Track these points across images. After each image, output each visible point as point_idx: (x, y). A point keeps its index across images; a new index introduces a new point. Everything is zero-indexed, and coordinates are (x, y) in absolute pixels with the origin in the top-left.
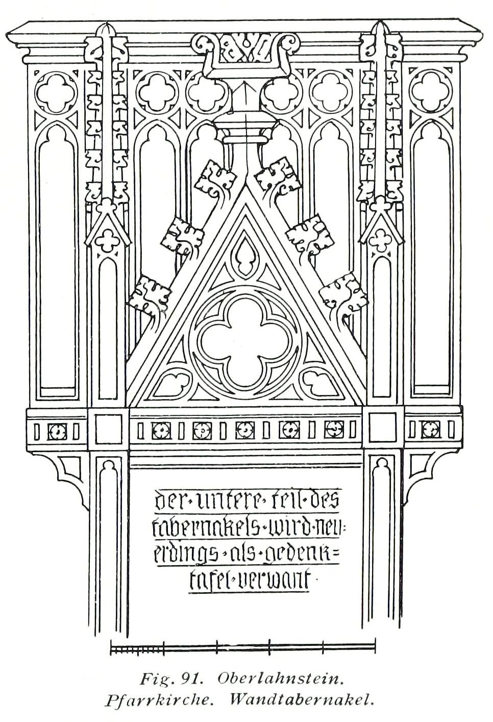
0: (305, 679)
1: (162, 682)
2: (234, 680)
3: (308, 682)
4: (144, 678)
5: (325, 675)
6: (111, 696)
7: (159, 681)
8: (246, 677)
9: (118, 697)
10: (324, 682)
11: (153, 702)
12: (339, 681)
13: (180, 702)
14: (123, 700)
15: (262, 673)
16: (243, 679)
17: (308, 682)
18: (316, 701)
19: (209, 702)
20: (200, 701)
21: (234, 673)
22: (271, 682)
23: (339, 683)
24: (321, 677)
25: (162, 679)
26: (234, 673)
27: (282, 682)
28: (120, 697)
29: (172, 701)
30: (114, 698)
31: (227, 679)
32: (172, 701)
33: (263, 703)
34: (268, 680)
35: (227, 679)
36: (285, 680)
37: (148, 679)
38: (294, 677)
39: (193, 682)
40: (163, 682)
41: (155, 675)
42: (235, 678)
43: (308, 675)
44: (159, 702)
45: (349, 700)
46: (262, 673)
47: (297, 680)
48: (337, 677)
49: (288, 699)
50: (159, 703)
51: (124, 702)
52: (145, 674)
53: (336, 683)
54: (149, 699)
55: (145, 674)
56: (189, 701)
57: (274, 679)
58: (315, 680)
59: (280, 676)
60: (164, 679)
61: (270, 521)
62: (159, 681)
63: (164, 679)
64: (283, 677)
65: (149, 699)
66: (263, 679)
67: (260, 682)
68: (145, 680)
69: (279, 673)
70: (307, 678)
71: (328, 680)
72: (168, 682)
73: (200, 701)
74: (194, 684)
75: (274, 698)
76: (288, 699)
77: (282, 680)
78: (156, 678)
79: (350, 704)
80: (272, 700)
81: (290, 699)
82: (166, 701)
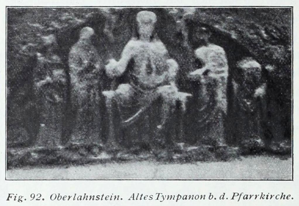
0: (100, 198)
1: (19, 199)
2: (59, 198)
3: (102, 199)
4: (9, 197)
5: (112, 195)
6: (234, 193)
7: (17, 199)
8: (66, 197)
9: (238, 194)
10: (267, 198)
11: (258, 197)
12: (120, 198)
13: (274, 198)
14: (241, 196)
15: (75, 194)
16: (107, 197)
17: (102, 199)
18: (256, 197)
19: (290, 198)
20: (286, 197)
21: (59, 194)
22: (81, 199)
23: (226, 199)
24: (67, 196)
25: (19, 197)
26: (59, 194)
27: (86, 199)
28: (240, 194)
29: (269, 197)
30: (236, 194)
31: (55, 198)
32: (269, 197)
33: (284, 199)
34: (79, 198)
35: (55, 198)
36: (89, 198)
37: (11, 197)
38: (94, 196)
39: (232, 198)
40: (20, 199)
41: (15, 195)
42: (60, 197)
43: (102, 195)
44: (262, 197)
45: (262, 196)
46: (75, 194)
47: (95, 198)
48: (118, 196)
49: (221, 196)
50: (262, 198)
51: (242, 197)
52: (9, 194)
53: (118, 199)
54: (251, 195)
55: (9, 194)
56: (279, 197)
57: (82, 198)
58: (106, 198)
59: (86, 196)
60: (20, 197)
61: (138, 194)
62: (17, 199)
63: (20, 197)
64: (87, 196)
65: (256, 195)
66: (76, 198)
67: (74, 199)
68: (10, 198)
69: (85, 194)
70: (101, 197)
71: (113, 198)
72: (23, 199)
73: (286, 197)
74: (233, 200)
75: (224, 196)
76: (221, 196)
77: (87, 198)
78: (16, 197)
79: (263, 198)
80: (222, 196)
81: (246, 196)
82: (265, 197)
